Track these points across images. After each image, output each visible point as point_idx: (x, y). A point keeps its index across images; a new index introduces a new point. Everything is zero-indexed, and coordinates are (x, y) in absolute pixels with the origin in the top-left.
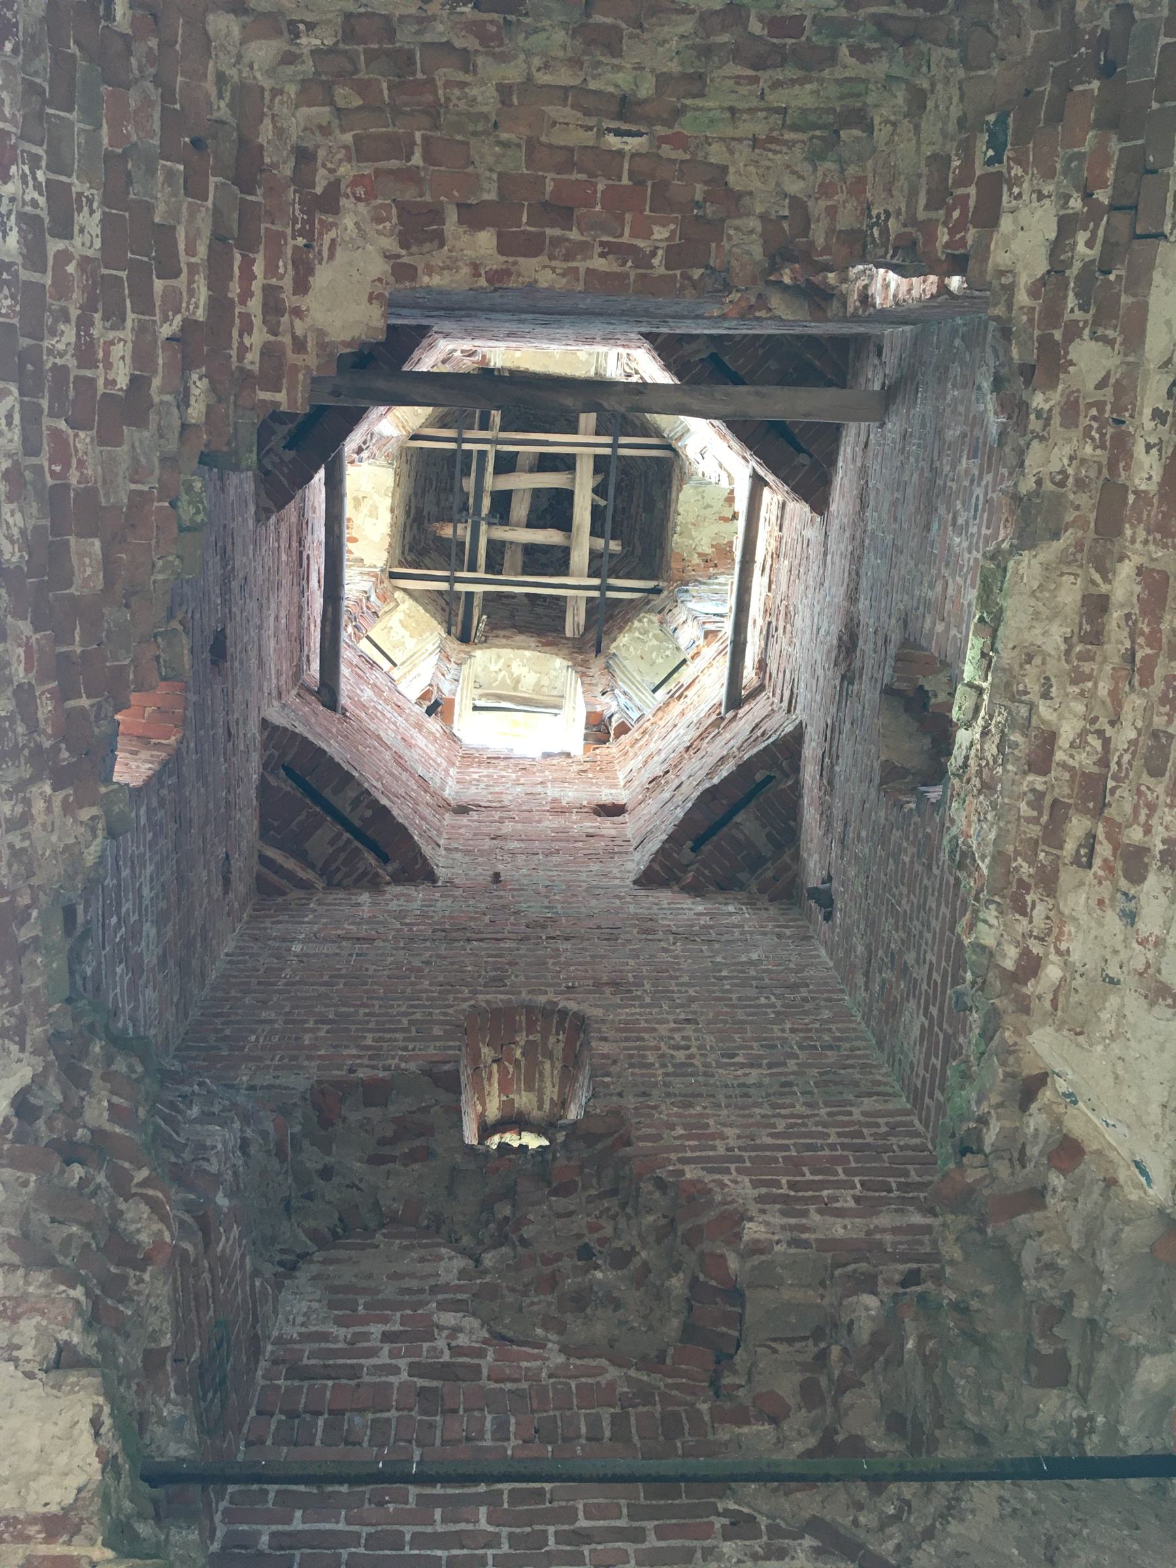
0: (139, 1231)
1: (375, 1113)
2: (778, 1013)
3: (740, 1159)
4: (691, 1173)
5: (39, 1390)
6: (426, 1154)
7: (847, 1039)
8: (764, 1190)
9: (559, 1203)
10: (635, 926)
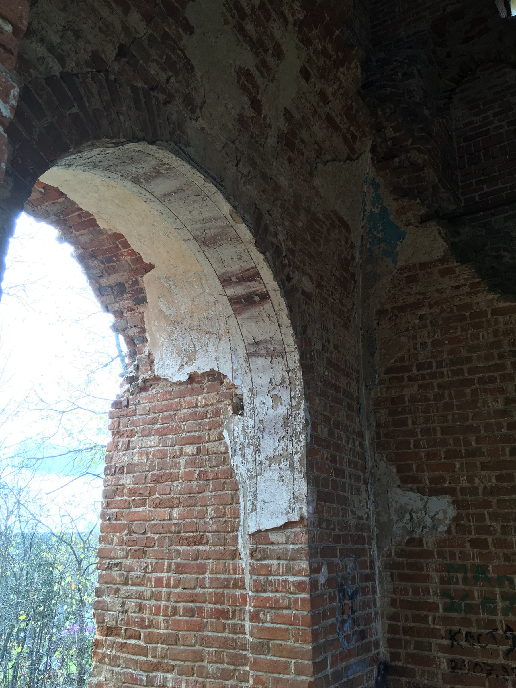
0: (417, 160)
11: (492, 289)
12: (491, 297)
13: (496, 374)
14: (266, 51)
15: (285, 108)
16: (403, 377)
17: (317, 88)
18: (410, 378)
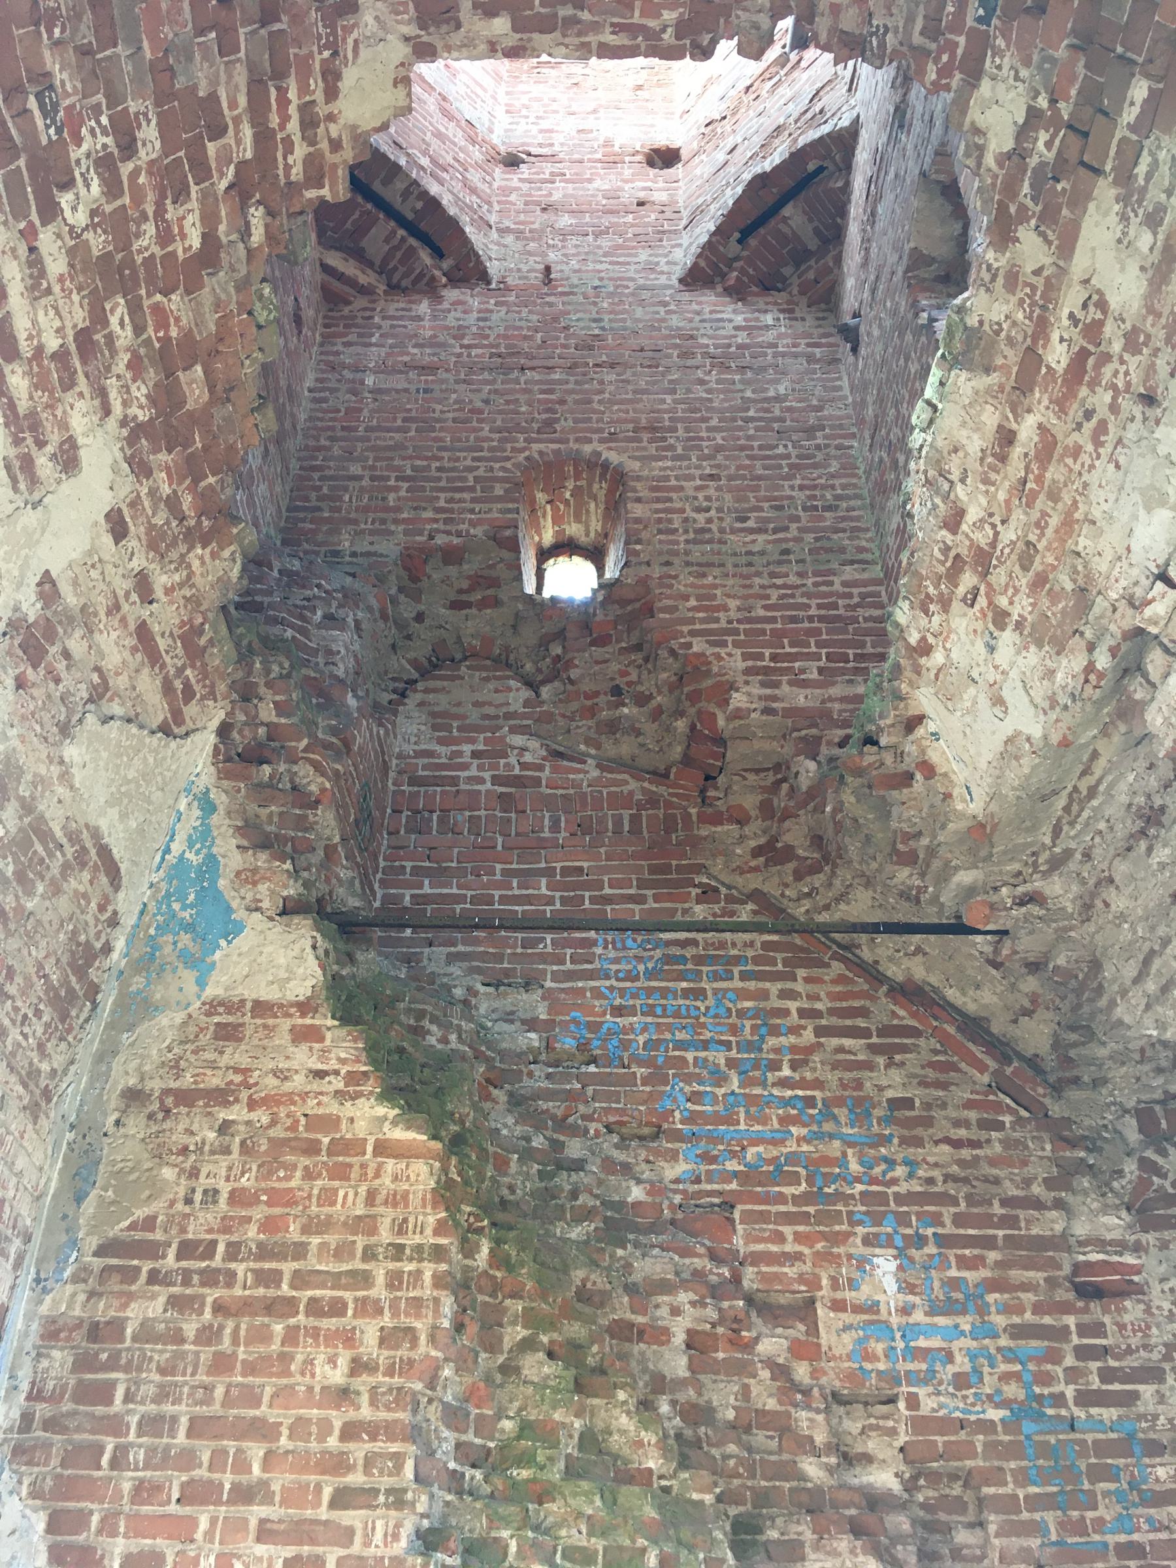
1: (452, 570)
2: (791, 466)
3: (736, 632)
4: (698, 646)
5: (279, 929)
6: (496, 603)
7: (848, 498)
8: (750, 663)
9: (598, 652)
10: (676, 346)
11: (388, 1095)
12: (381, 1111)
13: (348, 1296)
14: (41, 444)
15: (47, 572)
16: (138, 1269)
17: (136, 564)
18: (154, 1277)
